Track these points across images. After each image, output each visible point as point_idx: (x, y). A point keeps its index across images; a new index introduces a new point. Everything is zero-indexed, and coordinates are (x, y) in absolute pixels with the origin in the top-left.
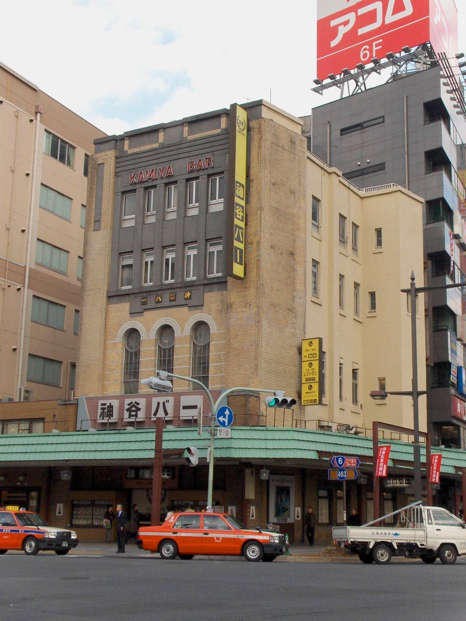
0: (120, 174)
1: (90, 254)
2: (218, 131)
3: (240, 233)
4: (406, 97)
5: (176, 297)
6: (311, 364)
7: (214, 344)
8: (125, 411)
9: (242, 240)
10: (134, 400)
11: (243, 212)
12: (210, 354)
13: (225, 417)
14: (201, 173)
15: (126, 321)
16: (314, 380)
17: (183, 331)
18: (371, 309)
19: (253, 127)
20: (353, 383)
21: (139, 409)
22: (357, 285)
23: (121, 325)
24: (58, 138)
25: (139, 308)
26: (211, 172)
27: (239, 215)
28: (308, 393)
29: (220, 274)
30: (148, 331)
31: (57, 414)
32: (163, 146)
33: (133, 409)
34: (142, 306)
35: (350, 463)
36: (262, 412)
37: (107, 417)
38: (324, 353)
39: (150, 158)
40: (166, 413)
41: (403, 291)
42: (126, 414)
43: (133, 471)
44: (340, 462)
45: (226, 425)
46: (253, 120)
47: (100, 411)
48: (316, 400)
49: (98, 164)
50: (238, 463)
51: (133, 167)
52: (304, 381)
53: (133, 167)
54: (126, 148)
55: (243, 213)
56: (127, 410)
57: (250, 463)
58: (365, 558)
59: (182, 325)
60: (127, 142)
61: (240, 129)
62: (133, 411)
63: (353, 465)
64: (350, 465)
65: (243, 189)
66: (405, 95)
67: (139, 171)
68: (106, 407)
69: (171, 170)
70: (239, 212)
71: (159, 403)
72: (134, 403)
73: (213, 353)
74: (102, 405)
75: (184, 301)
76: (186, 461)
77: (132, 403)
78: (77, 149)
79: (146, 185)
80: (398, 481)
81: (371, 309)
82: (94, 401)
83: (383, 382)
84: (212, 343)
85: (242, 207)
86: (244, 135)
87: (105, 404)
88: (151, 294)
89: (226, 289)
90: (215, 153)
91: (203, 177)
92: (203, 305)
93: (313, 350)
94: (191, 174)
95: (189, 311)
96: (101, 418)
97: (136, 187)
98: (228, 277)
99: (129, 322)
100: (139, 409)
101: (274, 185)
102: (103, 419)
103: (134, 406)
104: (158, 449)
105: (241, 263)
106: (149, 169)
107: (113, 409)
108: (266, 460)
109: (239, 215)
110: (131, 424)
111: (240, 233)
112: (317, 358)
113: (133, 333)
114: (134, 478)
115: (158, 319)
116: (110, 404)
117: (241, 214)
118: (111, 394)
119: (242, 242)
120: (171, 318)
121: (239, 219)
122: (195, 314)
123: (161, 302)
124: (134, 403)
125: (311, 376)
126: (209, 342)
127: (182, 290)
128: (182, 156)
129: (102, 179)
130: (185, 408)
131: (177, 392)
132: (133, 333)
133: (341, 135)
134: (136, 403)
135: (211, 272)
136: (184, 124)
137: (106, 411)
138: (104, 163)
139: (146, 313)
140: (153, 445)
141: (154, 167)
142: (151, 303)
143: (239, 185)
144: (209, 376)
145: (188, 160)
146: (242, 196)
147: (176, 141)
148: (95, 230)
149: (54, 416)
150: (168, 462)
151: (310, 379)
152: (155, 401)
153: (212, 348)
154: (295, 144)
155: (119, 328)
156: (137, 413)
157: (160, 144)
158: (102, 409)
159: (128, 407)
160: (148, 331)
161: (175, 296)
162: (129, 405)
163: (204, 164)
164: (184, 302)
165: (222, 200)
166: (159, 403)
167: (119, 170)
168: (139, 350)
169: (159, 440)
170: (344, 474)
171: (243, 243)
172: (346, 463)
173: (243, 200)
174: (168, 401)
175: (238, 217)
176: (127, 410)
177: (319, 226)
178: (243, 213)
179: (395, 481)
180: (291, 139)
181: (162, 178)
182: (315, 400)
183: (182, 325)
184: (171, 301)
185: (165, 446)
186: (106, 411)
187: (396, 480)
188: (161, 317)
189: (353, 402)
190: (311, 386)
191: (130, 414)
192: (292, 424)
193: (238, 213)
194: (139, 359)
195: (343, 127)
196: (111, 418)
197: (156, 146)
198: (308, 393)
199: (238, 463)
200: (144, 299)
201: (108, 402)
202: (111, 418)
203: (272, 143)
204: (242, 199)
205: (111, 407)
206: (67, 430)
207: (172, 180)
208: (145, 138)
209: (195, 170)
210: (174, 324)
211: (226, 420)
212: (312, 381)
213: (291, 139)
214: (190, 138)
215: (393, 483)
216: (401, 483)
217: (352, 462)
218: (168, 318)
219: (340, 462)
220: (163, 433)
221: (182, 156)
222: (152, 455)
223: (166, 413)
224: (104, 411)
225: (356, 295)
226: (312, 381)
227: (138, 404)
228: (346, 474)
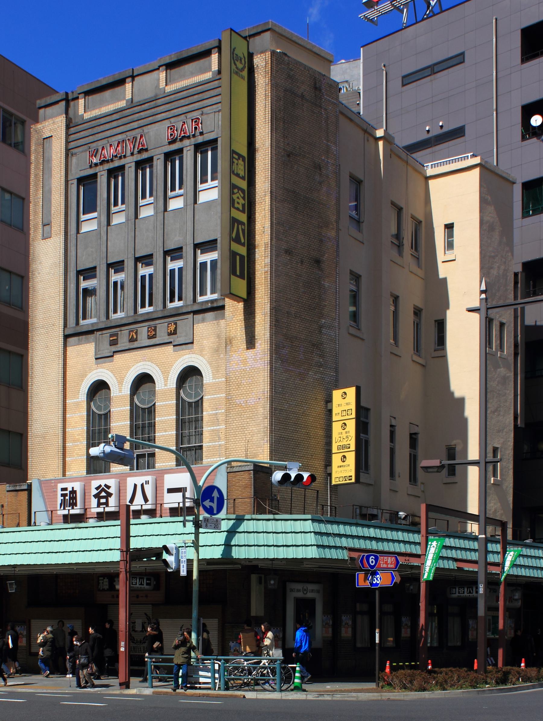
0: (74, 151)
1: (39, 273)
2: (208, 75)
3: (241, 231)
4: (496, 19)
5: (156, 332)
6: (345, 424)
7: (208, 400)
8: (93, 498)
9: (243, 241)
10: (103, 482)
11: (244, 198)
12: (204, 413)
13: (212, 500)
14: (186, 142)
15: (91, 370)
16: (349, 448)
17: (165, 384)
18: (438, 346)
19: (257, 66)
20: (410, 454)
21: (110, 495)
22: (417, 312)
23: (83, 376)
24: (11, 115)
25: (107, 350)
26: (200, 139)
27: (238, 203)
28: (340, 467)
29: (215, 296)
30: (120, 383)
31: (5, 506)
32: (132, 104)
33: (103, 494)
34: (113, 347)
35: (386, 563)
36: (275, 495)
37: (69, 507)
38: (367, 410)
39: (114, 124)
40: (146, 500)
41: (470, 310)
42: (94, 502)
43: (106, 580)
44: (372, 562)
45: (215, 512)
46: (257, 55)
47: (60, 499)
48: (351, 476)
49: (44, 139)
50: (240, 567)
51: (91, 139)
52: (334, 449)
53: (91, 139)
54: (81, 111)
55: (245, 201)
56: (96, 496)
57: (256, 567)
58: (535, 654)
59: (166, 374)
60: (81, 102)
61: (237, 68)
62: (103, 497)
63: (389, 566)
64: (385, 566)
65: (243, 163)
66: (494, 18)
67: (100, 143)
68: (68, 492)
69: (143, 140)
70: (238, 198)
71: (135, 486)
72: (103, 486)
73: (207, 413)
74: (63, 489)
75: (167, 337)
76: (163, 564)
77: (100, 486)
78: (27, 123)
79: (111, 165)
80: (466, 589)
81: (438, 346)
82: (53, 485)
83: (414, 436)
84: (206, 397)
85: (243, 191)
86: (243, 78)
87: (66, 489)
88: (123, 328)
89: (223, 317)
90: (205, 110)
91: (189, 148)
92: (192, 343)
93: (347, 404)
94: (171, 146)
95: (174, 351)
96: (62, 508)
97: (97, 169)
98: (227, 299)
99: (95, 371)
100: (110, 495)
101: (289, 156)
102: (64, 509)
103: (103, 490)
104: (126, 549)
105: (242, 277)
106: (114, 141)
107: (76, 495)
108: (273, 562)
109: (238, 203)
110: (101, 517)
111: (241, 231)
112: (354, 416)
113: (99, 388)
114: (108, 590)
115: (133, 364)
116: (73, 488)
117: (241, 201)
118: (75, 475)
119: (243, 245)
120: (149, 363)
121: (238, 209)
122: (183, 355)
123: (136, 340)
124: (103, 486)
125: (345, 443)
126: (202, 397)
127: (163, 321)
128: (159, 117)
129: (50, 160)
130: (170, 491)
131: (161, 469)
132: (99, 388)
133: (403, 85)
134: (106, 485)
135: (203, 293)
136: (161, 68)
137: (67, 498)
138: (52, 136)
139: (117, 357)
140: (117, 543)
141: (120, 137)
142: (124, 342)
143: (237, 157)
144: (204, 445)
145: (167, 124)
146: (242, 173)
147: (150, 95)
148: (44, 238)
149: (3, 506)
150: (137, 566)
151: (344, 447)
152: (131, 482)
153: (205, 405)
154: (320, 90)
155: (83, 380)
156: (107, 501)
157: (127, 101)
158: (62, 495)
159: (96, 492)
160: (120, 383)
161: (155, 330)
162: (97, 489)
163: (189, 128)
164: (167, 339)
165: (216, 183)
166: (135, 486)
167: (72, 145)
168: (110, 411)
169: (126, 536)
170: (377, 579)
171: (244, 246)
172: (380, 564)
173: (244, 180)
174: (147, 482)
175: (236, 205)
176: (96, 496)
177: (361, 220)
178: (245, 201)
179: (461, 590)
180: (315, 84)
181: (132, 154)
182: (350, 476)
183: (166, 374)
184: (150, 338)
185: (135, 544)
186: (67, 498)
187: (455, 588)
188: (137, 363)
189: (410, 481)
190: (344, 457)
191: (99, 501)
192: (335, 511)
193: (237, 200)
194: (110, 424)
195: (404, 73)
196: (75, 508)
197: (122, 104)
198: (340, 467)
199: (240, 567)
200: (115, 338)
201: (69, 486)
202: (75, 508)
203: (286, 90)
204: (243, 178)
205: (73, 492)
206: (18, 525)
207: (145, 155)
208: (107, 94)
209: (177, 138)
210: (155, 371)
211: (215, 506)
212: (346, 450)
213: (315, 84)
214: (169, 89)
215: (459, 593)
216: (470, 593)
217: (389, 561)
218: (147, 363)
219: (372, 562)
220: (131, 526)
221: (159, 117)
222: (116, 556)
223: (146, 500)
224: (64, 498)
225: (417, 326)
226: (346, 450)
227: (109, 487)
228: (380, 579)
